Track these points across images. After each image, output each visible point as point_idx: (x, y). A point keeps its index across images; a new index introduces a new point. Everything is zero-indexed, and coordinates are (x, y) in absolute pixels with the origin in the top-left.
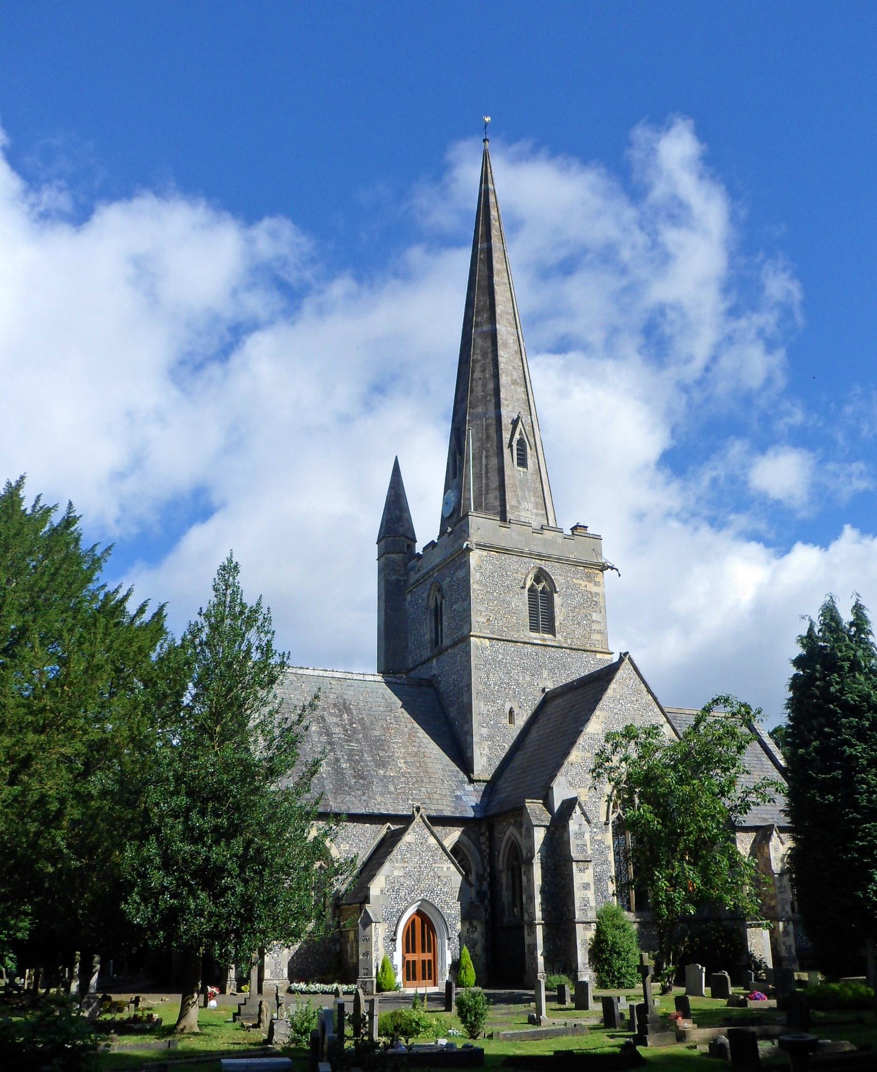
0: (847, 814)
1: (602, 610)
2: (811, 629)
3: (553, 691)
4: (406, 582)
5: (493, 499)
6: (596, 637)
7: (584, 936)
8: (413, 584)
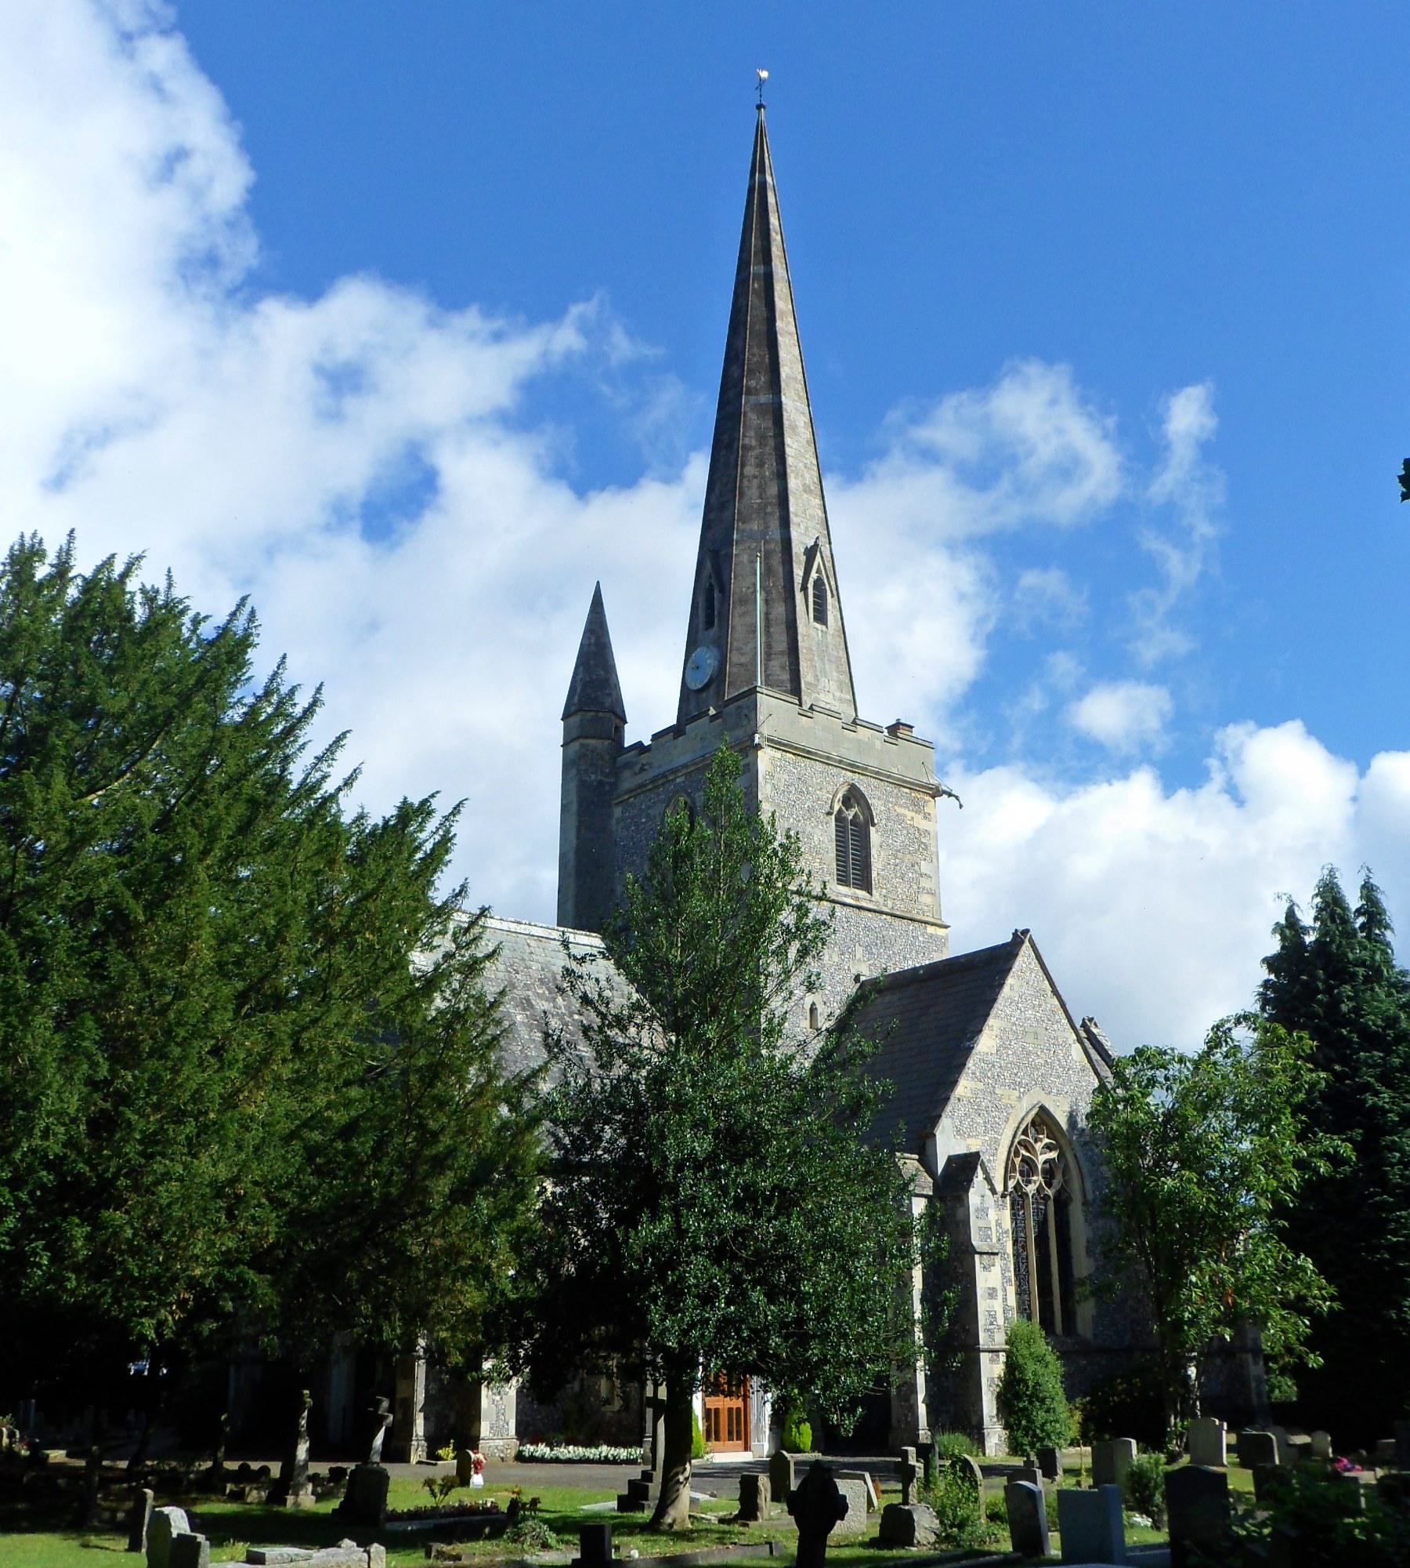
0: (1373, 1195)
1: (933, 859)
2: (1290, 915)
3: (874, 982)
4: (614, 786)
5: (779, 663)
6: (925, 899)
7: (992, 1370)
8: (631, 791)
